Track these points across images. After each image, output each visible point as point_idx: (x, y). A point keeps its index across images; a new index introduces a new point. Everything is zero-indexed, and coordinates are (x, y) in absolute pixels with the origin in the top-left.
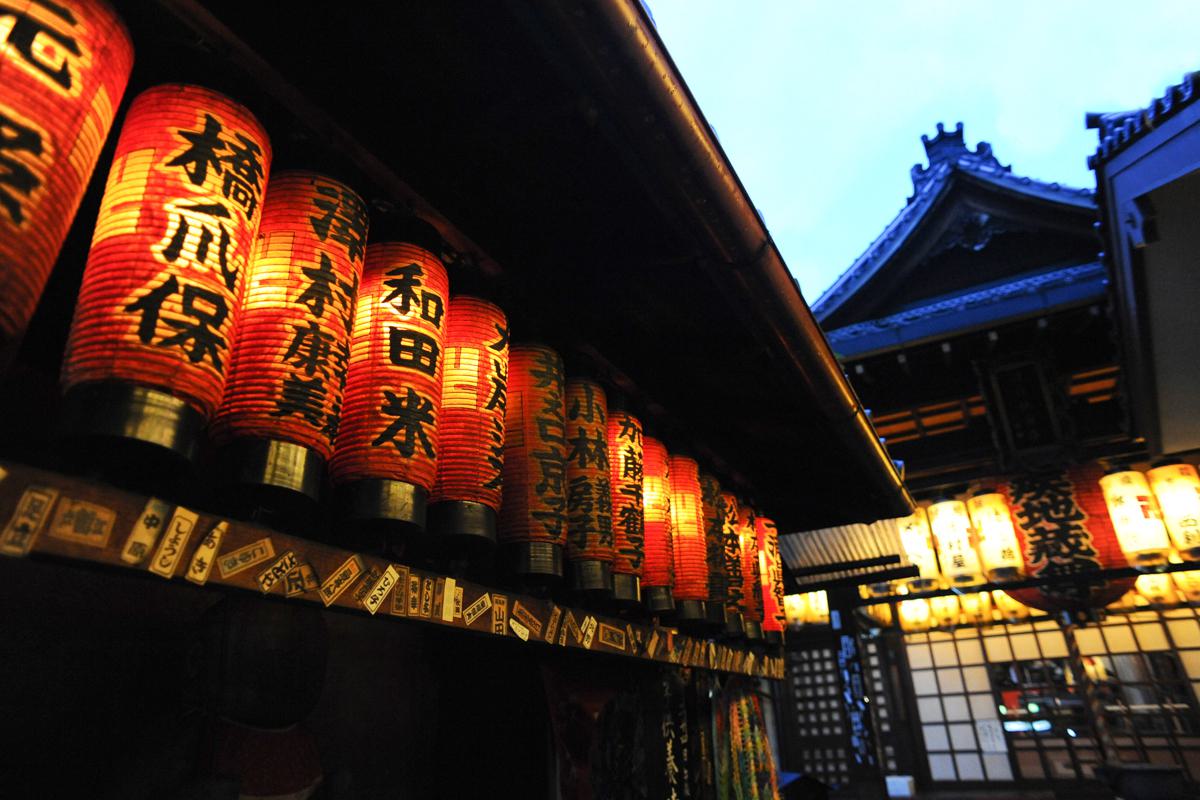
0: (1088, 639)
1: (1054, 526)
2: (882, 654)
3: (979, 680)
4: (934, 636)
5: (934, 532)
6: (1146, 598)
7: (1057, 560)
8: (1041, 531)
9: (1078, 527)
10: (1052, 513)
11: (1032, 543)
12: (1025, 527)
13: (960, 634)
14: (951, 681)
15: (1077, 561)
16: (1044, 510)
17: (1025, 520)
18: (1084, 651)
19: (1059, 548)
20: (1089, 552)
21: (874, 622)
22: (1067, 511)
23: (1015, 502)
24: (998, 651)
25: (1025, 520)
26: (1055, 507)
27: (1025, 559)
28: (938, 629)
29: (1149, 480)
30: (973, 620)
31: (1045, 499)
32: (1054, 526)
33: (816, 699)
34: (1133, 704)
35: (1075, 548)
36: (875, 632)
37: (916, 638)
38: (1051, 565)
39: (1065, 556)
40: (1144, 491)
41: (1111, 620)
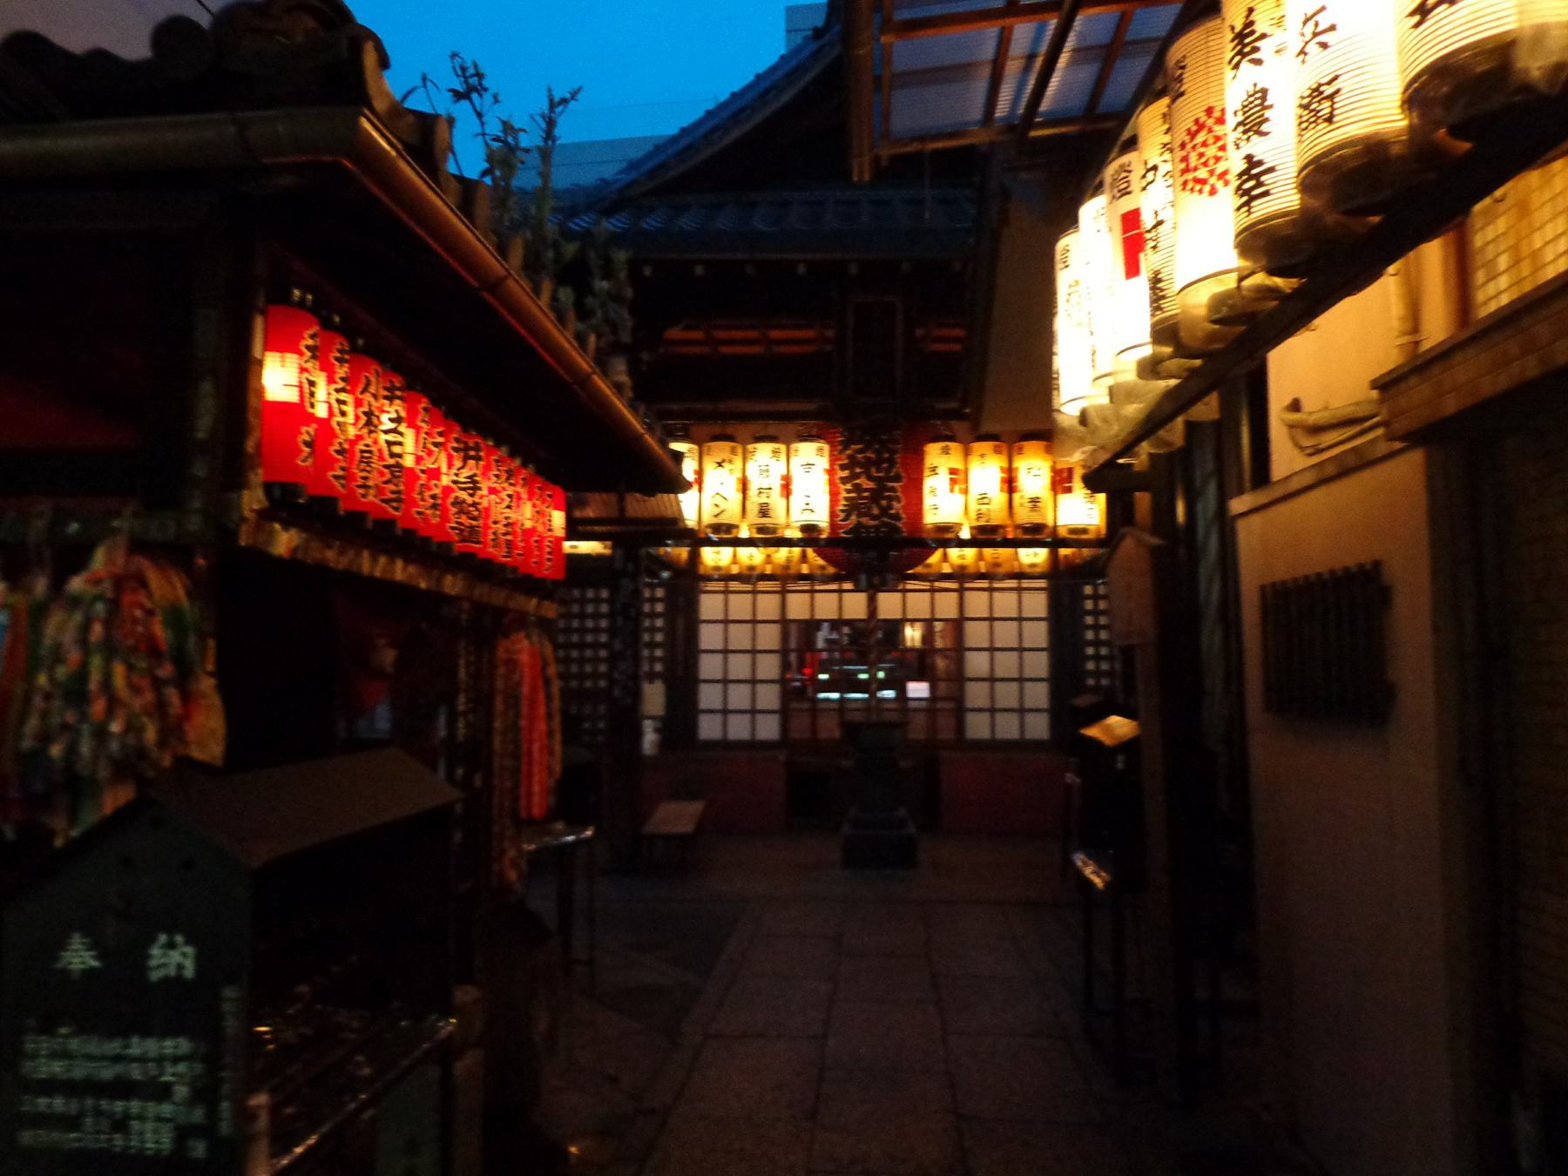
0: (889, 605)
1: (871, 485)
2: (669, 600)
3: (769, 637)
4: (734, 585)
5: (740, 496)
6: (952, 566)
7: (864, 520)
8: (857, 488)
9: (893, 489)
10: (873, 470)
11: (846, 499)
12: (844, 480)
13: (762, 585)
14: (739, 666)
15: (884, 524)
16: (866, 465)
17: (846, 473)
18: (969, 643)
19: (869, 509)
20: (897, 517)
21: (667, 564)
22: (888, 470)
23: (841, 452)
24: (798, 606)
25: (846, 473)
26: (877, 463)
27: (833, 514)
28: (738, 578)
29: (967, 453)
30: (779, 572)
31: (870, 454)
32: (871, 485)
33: (582, 646)
34: (266, 323)
35: (884, 511)
36: (665, 575)
37: (712, 586)
38: (859, 525)
39: (874, 518)
40: (959, 465)
41: (911, 585)
